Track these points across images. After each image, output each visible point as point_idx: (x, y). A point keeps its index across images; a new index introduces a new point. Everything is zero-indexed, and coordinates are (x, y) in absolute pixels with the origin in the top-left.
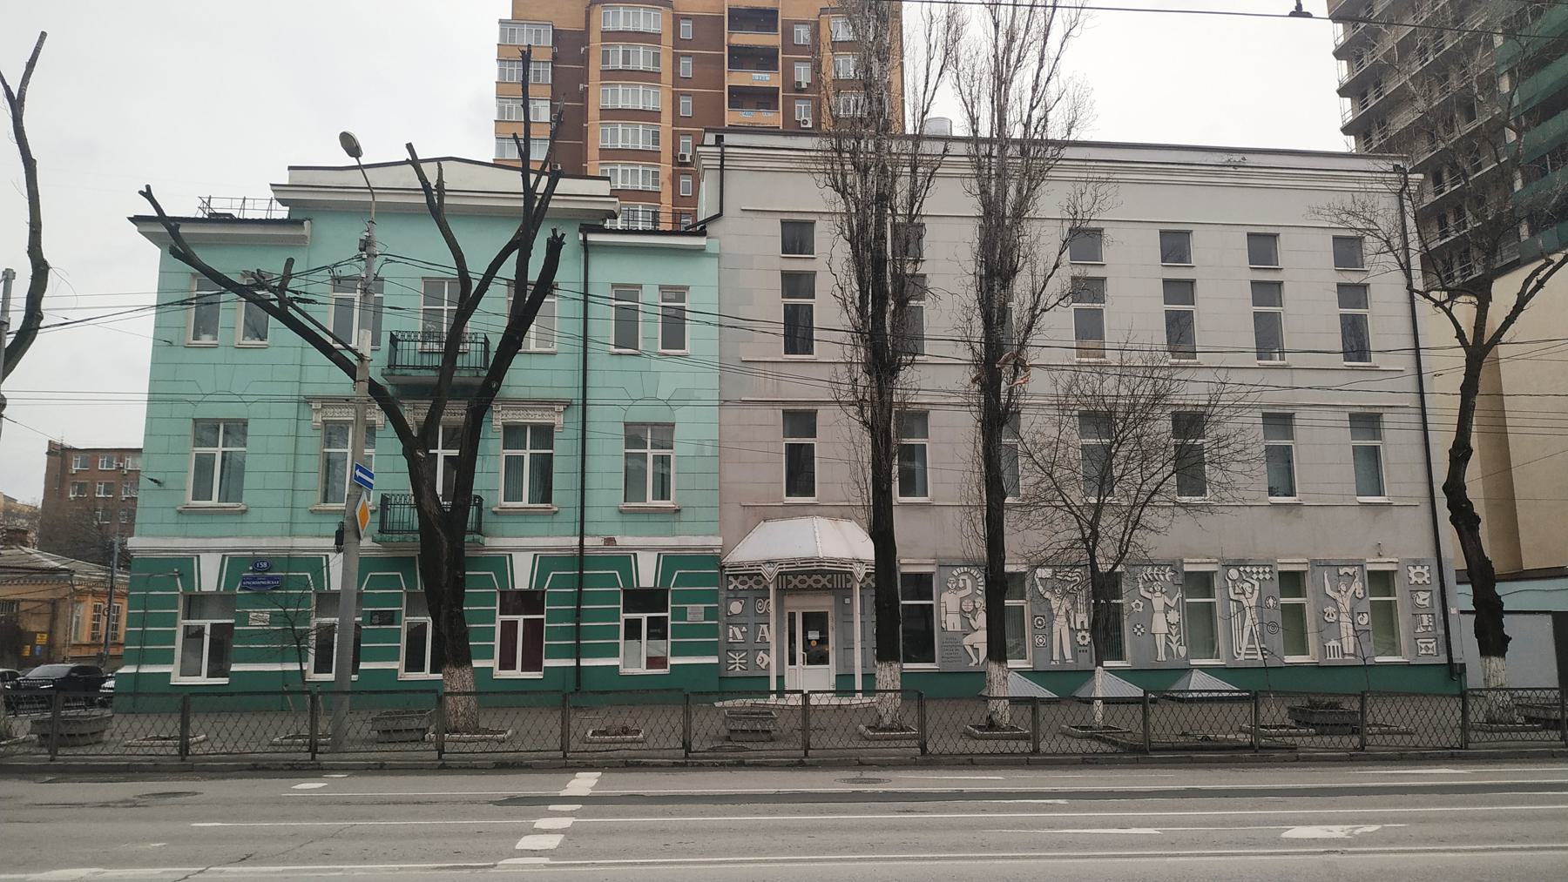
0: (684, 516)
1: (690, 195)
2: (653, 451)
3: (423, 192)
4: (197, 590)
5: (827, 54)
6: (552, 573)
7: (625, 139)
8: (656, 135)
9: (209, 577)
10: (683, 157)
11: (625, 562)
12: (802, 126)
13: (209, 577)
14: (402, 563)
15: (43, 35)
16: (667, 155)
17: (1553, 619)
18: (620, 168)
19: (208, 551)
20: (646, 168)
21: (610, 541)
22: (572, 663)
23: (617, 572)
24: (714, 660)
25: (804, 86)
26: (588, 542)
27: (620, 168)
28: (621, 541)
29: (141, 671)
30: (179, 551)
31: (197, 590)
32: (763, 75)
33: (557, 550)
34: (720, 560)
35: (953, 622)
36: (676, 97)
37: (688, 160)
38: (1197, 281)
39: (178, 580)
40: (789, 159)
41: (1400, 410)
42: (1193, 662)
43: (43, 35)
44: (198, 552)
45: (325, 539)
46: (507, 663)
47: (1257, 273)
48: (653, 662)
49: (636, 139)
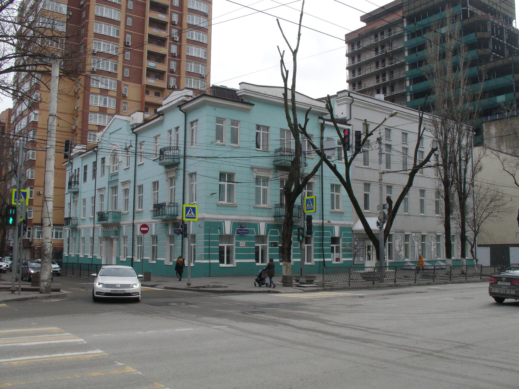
0: (344, 215)
1: (129, 59)
2: (263, 187)
3: (296, 102)
4: (224, 233)
5: (185, 12)
6: (278, 230)
7: (105, 31)
8: (118, 31)
9: (228, 230)
10: (128, 43)
11: (332, 229)
12: (175, 39)
13: (228, 230)
14: (277, 226)
15: (278, 47)
16: (122, 41)
17: (490, 248)
18: (102, 43)
19: (227, 220)
20: (105, 43)
21: (329, 222)
22: (322, 260)
23: (278, 230)
24: (351, 259)
25: (176, 23)
26: (325, 222)
27: (102, 43)
28: (332, 222)
29: (211, 262)
30: (218, 219)
31: (224, 233)
32: (163, 16)
33: (316, 224)
34: (351, 228)
35: (397, 248)
36: (127, 16)
37: (130, 44)
38: (409, 149)
39: (218, 230)
40: (365, 104)
41: (375, 183)
42: (438, 259)
43: (278, 47)
44: (224, 220)
45: (259, 217)
46: (222, 261)
47: (386, 141)
48: (338, 260)
49: (110, 32)
